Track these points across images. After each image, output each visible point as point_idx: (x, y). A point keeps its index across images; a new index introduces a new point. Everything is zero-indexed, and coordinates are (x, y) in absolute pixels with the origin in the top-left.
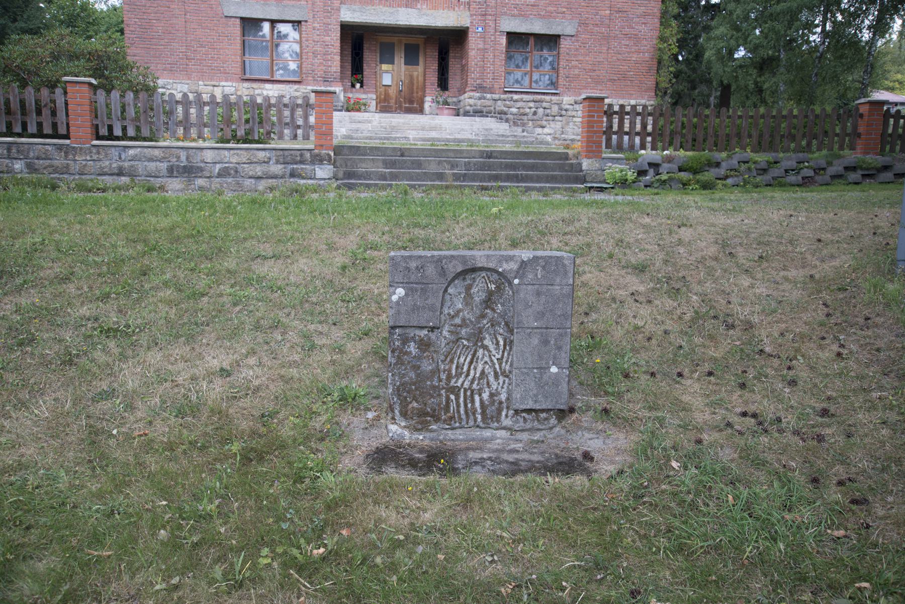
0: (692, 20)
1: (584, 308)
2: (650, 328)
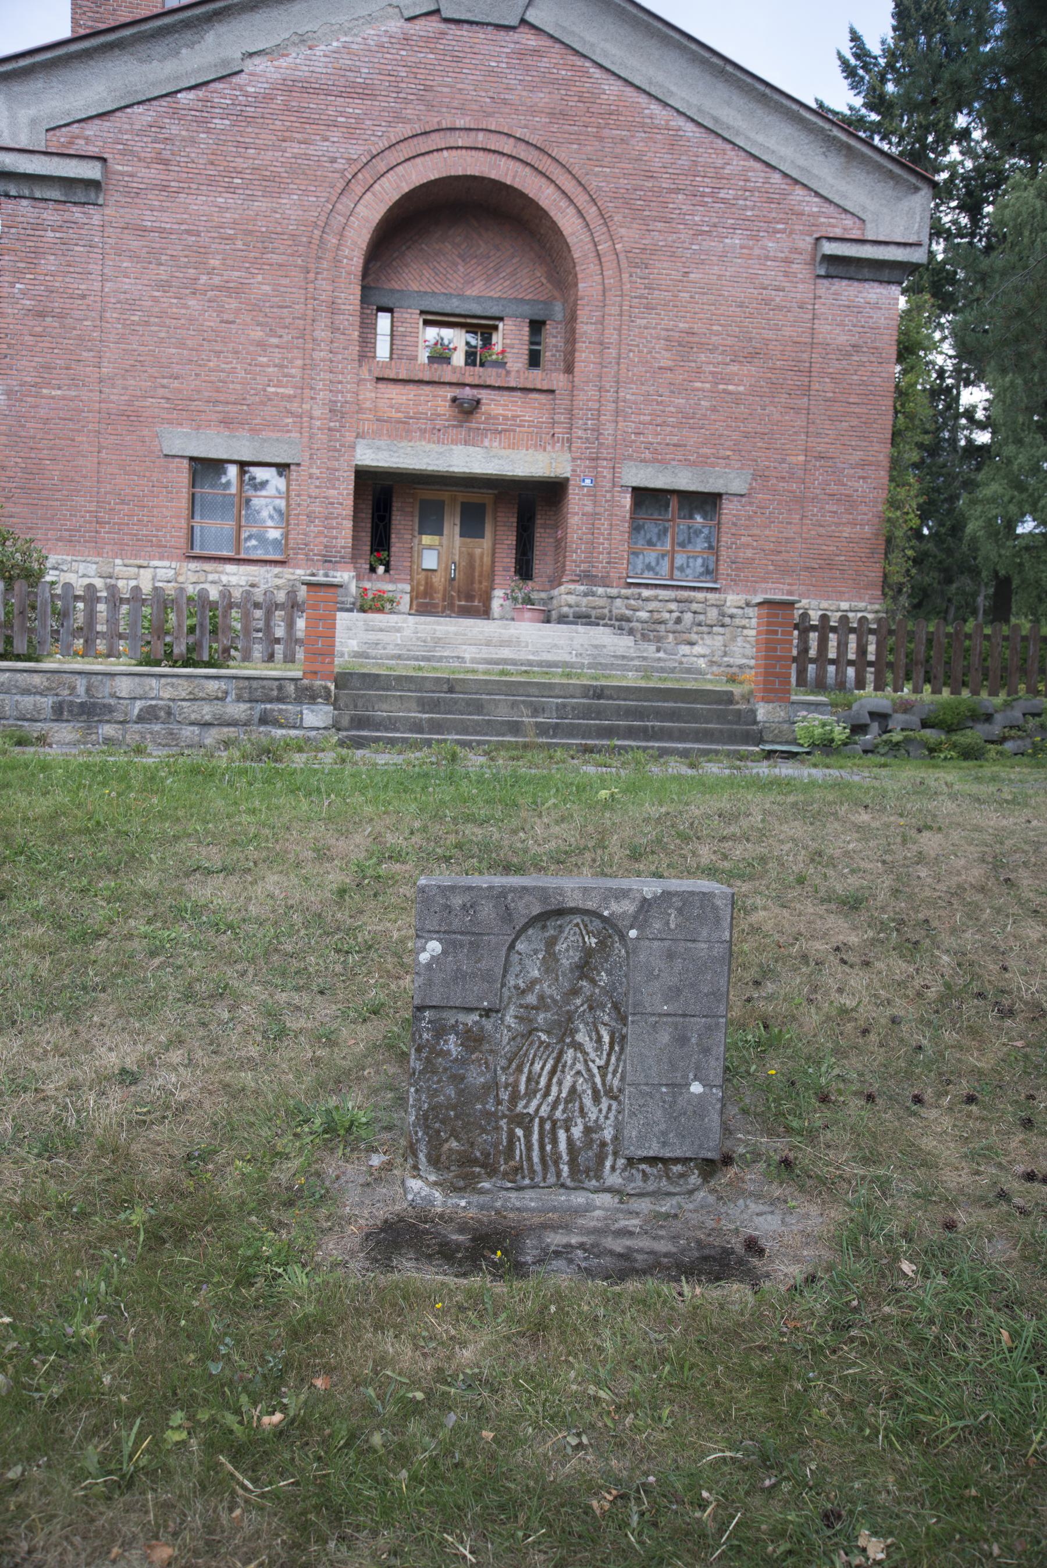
0: (944, 471)
1: (753, 973)
2: (867, 1011)
